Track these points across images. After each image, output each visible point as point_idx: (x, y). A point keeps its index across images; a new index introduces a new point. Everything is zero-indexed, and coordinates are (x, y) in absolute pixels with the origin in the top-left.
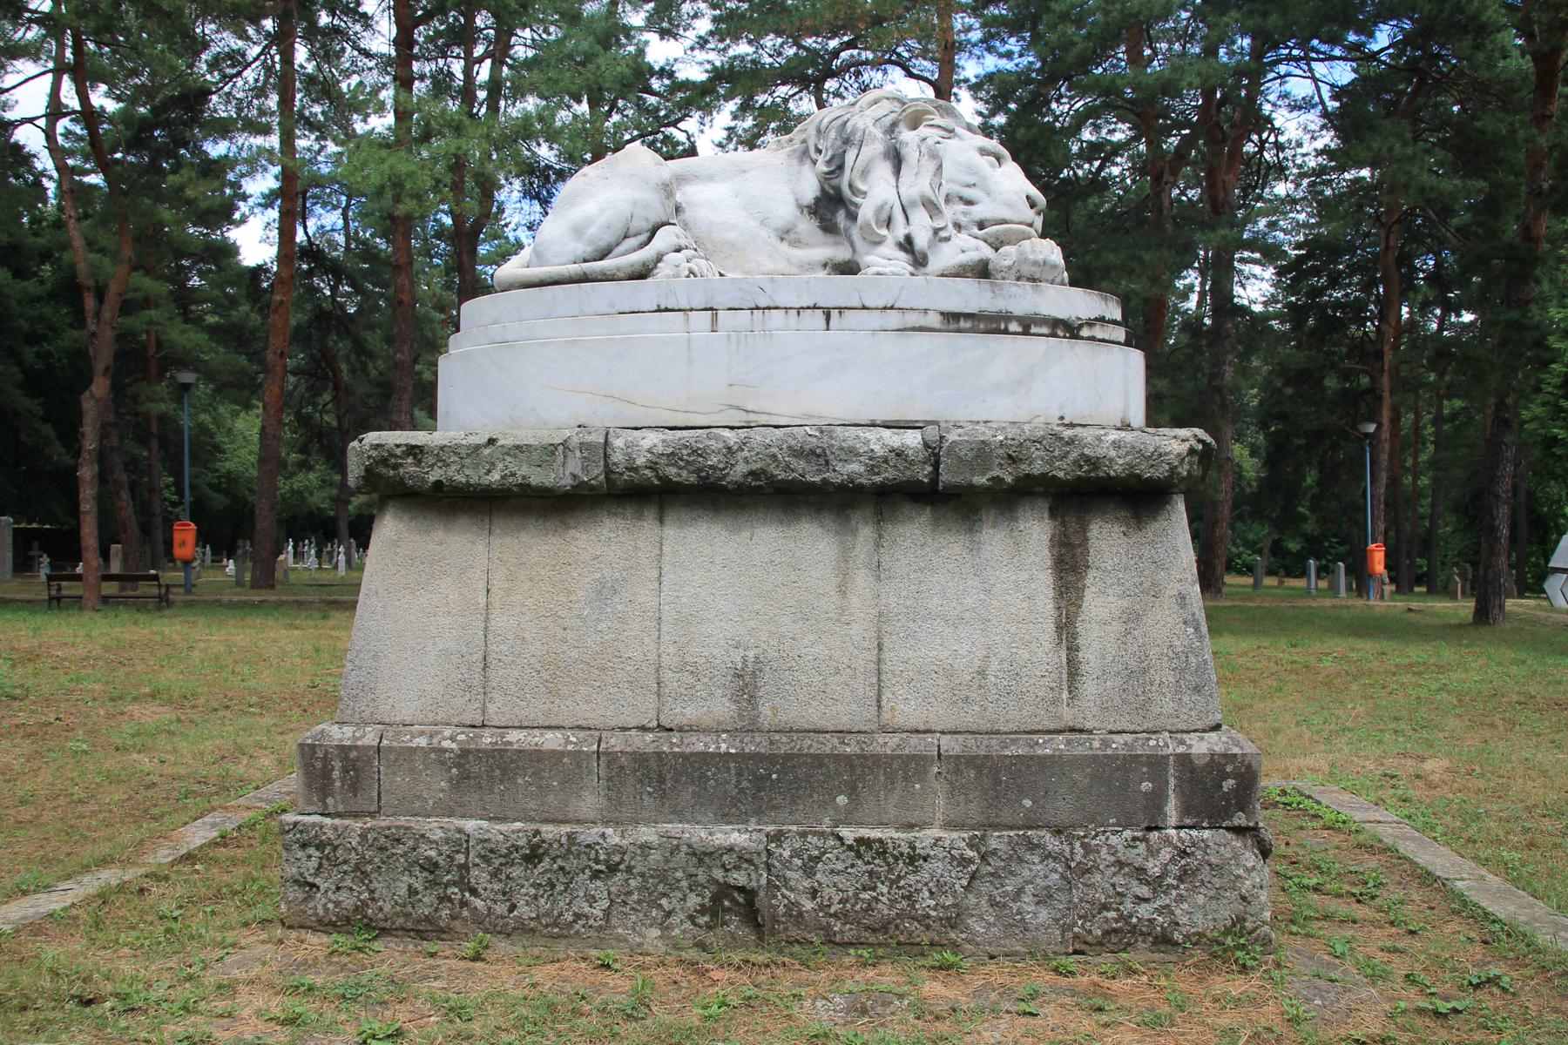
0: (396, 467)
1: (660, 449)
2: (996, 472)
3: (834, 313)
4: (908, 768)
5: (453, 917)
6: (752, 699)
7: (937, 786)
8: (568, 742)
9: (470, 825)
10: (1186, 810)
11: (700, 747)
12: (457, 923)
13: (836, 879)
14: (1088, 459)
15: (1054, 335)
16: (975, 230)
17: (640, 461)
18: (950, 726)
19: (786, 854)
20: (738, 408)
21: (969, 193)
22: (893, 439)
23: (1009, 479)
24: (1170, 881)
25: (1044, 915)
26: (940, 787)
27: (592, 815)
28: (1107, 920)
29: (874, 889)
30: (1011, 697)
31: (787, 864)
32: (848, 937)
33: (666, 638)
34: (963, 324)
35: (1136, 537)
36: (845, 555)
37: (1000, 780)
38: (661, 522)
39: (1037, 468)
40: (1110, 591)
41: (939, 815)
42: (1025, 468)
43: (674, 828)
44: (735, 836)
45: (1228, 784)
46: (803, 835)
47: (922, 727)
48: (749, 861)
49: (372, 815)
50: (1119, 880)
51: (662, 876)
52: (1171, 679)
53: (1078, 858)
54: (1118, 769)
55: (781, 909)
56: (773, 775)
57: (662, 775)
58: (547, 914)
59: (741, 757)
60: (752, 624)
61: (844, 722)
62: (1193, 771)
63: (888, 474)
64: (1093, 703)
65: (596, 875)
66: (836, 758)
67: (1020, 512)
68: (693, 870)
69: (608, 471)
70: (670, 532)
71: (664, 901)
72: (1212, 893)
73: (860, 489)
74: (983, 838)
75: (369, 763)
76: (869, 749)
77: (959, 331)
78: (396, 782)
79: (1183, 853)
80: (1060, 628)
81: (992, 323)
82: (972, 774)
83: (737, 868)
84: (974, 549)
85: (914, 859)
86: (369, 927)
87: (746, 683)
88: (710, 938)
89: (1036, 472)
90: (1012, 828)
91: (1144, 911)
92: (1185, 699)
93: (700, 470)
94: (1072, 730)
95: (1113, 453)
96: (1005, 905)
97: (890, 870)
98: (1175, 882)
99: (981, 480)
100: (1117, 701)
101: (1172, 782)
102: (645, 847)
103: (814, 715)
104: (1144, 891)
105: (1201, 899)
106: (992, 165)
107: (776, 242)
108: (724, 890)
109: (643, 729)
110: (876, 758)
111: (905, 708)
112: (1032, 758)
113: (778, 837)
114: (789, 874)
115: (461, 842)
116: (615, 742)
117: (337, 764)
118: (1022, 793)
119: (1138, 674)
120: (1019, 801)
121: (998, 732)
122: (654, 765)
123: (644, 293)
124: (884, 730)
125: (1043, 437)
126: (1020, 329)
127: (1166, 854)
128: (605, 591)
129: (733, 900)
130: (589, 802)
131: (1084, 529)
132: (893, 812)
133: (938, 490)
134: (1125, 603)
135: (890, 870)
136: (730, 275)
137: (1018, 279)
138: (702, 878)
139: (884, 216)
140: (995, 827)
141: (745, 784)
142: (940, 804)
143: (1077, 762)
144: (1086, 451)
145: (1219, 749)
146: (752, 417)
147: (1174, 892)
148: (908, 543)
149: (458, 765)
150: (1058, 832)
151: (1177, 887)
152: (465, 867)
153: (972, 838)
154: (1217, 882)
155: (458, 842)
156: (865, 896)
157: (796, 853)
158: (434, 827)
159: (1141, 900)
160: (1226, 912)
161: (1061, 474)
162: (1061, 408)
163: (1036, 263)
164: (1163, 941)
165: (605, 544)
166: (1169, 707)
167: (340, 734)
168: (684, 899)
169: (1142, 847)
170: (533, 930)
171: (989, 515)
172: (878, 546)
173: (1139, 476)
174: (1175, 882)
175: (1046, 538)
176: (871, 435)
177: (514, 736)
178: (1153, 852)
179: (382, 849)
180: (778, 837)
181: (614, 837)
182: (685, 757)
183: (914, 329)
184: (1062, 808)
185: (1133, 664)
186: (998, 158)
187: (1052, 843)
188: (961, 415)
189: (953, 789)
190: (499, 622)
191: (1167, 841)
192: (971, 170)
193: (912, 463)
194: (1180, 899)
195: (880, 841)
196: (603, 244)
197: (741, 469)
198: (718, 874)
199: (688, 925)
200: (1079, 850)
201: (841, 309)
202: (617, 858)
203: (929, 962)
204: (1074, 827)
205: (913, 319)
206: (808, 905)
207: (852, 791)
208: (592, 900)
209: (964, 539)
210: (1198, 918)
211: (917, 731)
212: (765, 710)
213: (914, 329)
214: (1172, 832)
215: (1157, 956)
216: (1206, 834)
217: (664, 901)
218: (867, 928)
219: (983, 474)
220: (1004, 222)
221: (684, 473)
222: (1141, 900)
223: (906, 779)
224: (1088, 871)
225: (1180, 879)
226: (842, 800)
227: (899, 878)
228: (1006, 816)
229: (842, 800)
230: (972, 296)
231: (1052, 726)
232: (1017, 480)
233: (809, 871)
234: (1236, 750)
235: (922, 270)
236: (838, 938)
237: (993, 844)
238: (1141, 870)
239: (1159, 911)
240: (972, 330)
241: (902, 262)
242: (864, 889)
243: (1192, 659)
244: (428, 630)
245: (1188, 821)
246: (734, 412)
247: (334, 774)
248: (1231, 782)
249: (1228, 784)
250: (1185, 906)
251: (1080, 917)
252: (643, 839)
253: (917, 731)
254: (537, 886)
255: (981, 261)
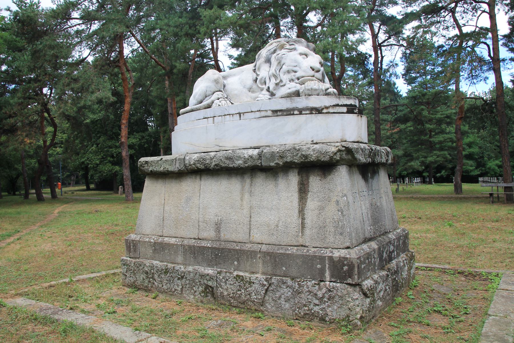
0: (144, 167)
1: (196, 159)
2: (277, 161)
3: (242, 114)
4: (252, 254)
5: (152, 287)
6: (219, 231)
7: (259, 260)
8: (176, 241)
9: (155, 262)
10: (332, 276)
11: (203, 245)
12: (152, 288)
13: (231, 286)
14: (304, 156)
15: (311, 113)
16: (297, 81)
17: (192, 163)
18: (268, 242)
19: (221, 278)
20: (218, 146)
21: (295, 69)
22: (251, 152)
23: (281, 163)
24: (325, 299)
25: (287, 306)
26: (260, 261)
27: (180, 262)
28: (305, 310)
29: (241, 291)
30: (285, 234)
31: (221, 280)
32: (235, 304)
33: (200, 213)
34: (279, 113)
35: (324, 181)
36: (243, 187)
37: (276, 260)
38: (201, 179)
39: (289, 159)
40: (315, 199)
41: (260, 270)
42: (285, 160)
43: (196, 267)
44: (210, 271)
45: (345, 268)
46: (226, 272)
47: (260, 242)
48: (212, 279)
49: (138, 258)
50: (309, 297)
51: (193, 280)
52: (333, 230)
53: (296, 288)
54: (310, 260)
55: (219, 294)
56: (220, 254)
57: (196, 252)
58: (169, 288)
59: (212, 248)
60: (220, 209)
61: (241, 239)
62: (334, 262)
63: (250, 163)
64: (309, 237)
65: (179, 279)
66: (235, 250)
67: (289, 174)
68: (200, 280)
69: (185, 165)
70: (203, 182)
71: (194, 288)
72: (339, 306)
73: (242, 168)
74: (271, 278)
75: (137, 245)
76: (243, 248)
77: (277, 116)
78: (142, 249)
79: (330, 291)
80: (299, 212)
81: (289, 112)
82: (269, 258)
83: (210, 280)
84: (276, 186)
85: (251, 283)
86: (136, 287)
87: (218, 227)
88: (205, 300)
89: (288, 161)
90: (280, 276)
91: (316, 309)
92: (337, 237)
93: (205, 165)
94: (302, 246)
95: (312, 153)
96: (276, 301)
97: (244, 286)
98: (327, 300)
99: (272, 164)
100: (316, 237)
101: (327, 266)
102: (189, 272)
103: (233, 237)
104: (317, 302)
105: (335, 307)
106: (304, 58)
107: (247, 92)
108: (207, 287)
109: (195, 239)
110: (244, 250)
111: (257, 236)
112: (285, 254)
113: (220, 273)
114: (222, 284)
115: (152, 267)
116: (186, 242)
117: (132, 244)
118: (282, 265)
119: (323, 227)
120: (281, 268)
121: (281, 245)
122: (193, 249)
123: (208, 112)
124: (251, 242)
125: (291, 149)
126: (298, 113)
127: (324, 290)
128: (188, 199)
129: (209, 290)
130: (180, 259)
131: (308, 179)
132: (248, 268)
133: (311, 167)
134: (319, 204)
135: (244, 286)
136: (235, 104)
137: (305, 95)
138: (202, 282)
139: (263, 81)
140: (276, 275)
141: (213, 256)
142: (260, 267)
143: (298, 256)
144: (303, 153)
145: (342, 255)
146: (221, 148)
147: (327, 304)
148: (259, 184)
149: (154, 246)
150: (293, 279)
151: (327, 302)
152: (153, 273)
153: (267, 278)
154: (341, 302)
155: (152, 267)
156: (239, 292)
157: (223, 278)
158: (147, 262)
159: (316, 305)
160: (343, 313)
161: (296, 161)
162: (312, 138)
163: (308, 90)
164: (322, 320)
165: (189, 186)
166: (332, 239)
167: (133, 236)
168: (198, 288)
169: (317, 287)
170: (167, 292)
171: (281, 175)
172: (251, 185)
173: (320, 160)
174: (327, 300)
175: (296, 182)
176: (245, 151)
177: (166, 239)
178: (320, 289)
179: (138, 267)
180: (220, 273)
181: (183, 268)
182: (199, 247)
183: (264, 117)
184: (294, 272)
185: (321, 224)
186: (306, 55)
187: (290, 282)
188: (277, 143)
189: (264, 262)
190: (167, 208)
191: (325, 285)
192: (296, 61)
193: (254, 160)
194: (329, 306)
195: (242, 276)
196: (199, 100)
197: (214, 164)
198: (206, 282)
199: (199, 296)
200: (297, 286)
201: (243, 113)
202: (183, 275)
203: (254, 315)
204: (298, 278)
205: (263, 114)
206: (225, 293)
207: (238, 261)
208: (178, 285)
209: (274, 183)
210: (334, 314)
211: (259, 243)
212: (222, 235)
213: (264, 117)
214: (328, 283)
215: (321, 325)
216: (338, 285)
217: (194, 288)
218: (240, 303)
219: (273, 162)
220: (303, 77)
221: (201, 166)
222: (316, 305)
223: (251, 258)
224: (300, 293)
225: (329, 299)
226: (236, 263)
227: (247, 288)
228: (278, 272)
229: (236, 263)
230: (285, 104)
231: (296, 244)
232: (284, 163)
233: (225, 282)
234: (348, 256)
235: (274, 97)
236: (232, 304)
237: (273, 281)
238: (316, 294)
239: (322, 309)
240: (282, 115)
241: (267, 95)
242: (238, 290)
243: (340, 223)
244: (163, 211)
245: (333, 280)
246: (217, 147)
247: (132, 247)
248: (346, 267)
249: (345, 268)
250: (330, 309)
251: (298, 308)
252: (189, 270)
253: (259, 243)
254: (167, 280)
255: (296, 91)
